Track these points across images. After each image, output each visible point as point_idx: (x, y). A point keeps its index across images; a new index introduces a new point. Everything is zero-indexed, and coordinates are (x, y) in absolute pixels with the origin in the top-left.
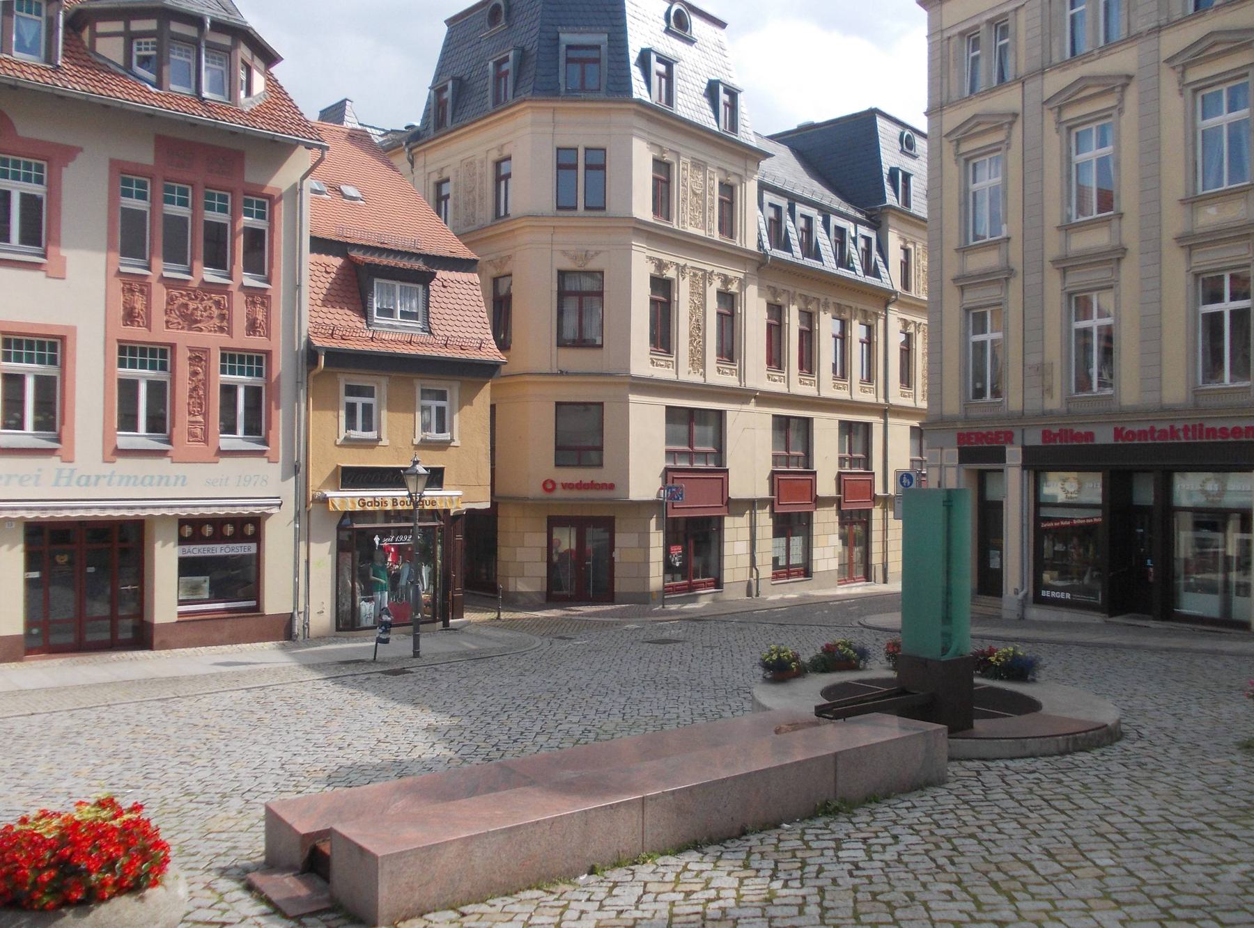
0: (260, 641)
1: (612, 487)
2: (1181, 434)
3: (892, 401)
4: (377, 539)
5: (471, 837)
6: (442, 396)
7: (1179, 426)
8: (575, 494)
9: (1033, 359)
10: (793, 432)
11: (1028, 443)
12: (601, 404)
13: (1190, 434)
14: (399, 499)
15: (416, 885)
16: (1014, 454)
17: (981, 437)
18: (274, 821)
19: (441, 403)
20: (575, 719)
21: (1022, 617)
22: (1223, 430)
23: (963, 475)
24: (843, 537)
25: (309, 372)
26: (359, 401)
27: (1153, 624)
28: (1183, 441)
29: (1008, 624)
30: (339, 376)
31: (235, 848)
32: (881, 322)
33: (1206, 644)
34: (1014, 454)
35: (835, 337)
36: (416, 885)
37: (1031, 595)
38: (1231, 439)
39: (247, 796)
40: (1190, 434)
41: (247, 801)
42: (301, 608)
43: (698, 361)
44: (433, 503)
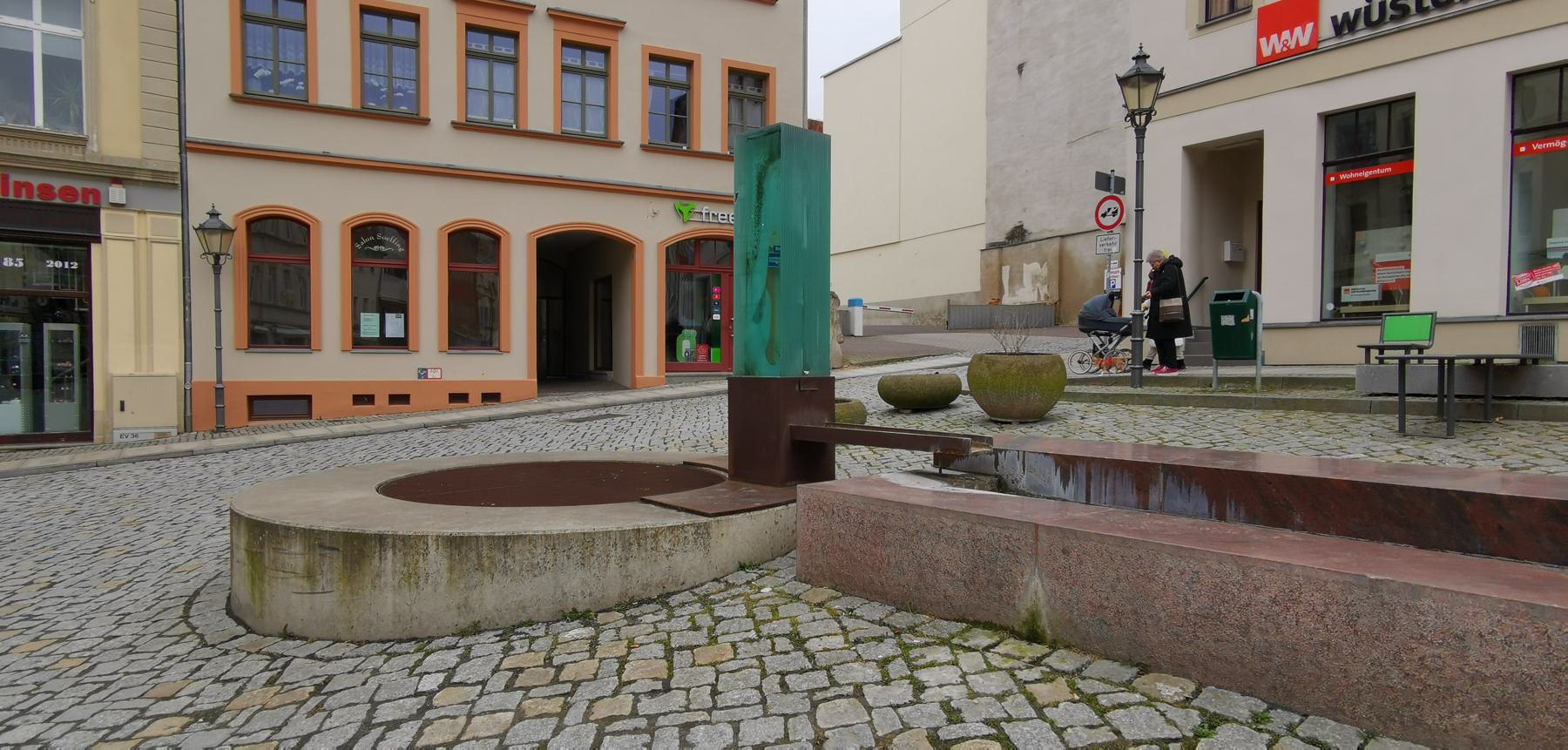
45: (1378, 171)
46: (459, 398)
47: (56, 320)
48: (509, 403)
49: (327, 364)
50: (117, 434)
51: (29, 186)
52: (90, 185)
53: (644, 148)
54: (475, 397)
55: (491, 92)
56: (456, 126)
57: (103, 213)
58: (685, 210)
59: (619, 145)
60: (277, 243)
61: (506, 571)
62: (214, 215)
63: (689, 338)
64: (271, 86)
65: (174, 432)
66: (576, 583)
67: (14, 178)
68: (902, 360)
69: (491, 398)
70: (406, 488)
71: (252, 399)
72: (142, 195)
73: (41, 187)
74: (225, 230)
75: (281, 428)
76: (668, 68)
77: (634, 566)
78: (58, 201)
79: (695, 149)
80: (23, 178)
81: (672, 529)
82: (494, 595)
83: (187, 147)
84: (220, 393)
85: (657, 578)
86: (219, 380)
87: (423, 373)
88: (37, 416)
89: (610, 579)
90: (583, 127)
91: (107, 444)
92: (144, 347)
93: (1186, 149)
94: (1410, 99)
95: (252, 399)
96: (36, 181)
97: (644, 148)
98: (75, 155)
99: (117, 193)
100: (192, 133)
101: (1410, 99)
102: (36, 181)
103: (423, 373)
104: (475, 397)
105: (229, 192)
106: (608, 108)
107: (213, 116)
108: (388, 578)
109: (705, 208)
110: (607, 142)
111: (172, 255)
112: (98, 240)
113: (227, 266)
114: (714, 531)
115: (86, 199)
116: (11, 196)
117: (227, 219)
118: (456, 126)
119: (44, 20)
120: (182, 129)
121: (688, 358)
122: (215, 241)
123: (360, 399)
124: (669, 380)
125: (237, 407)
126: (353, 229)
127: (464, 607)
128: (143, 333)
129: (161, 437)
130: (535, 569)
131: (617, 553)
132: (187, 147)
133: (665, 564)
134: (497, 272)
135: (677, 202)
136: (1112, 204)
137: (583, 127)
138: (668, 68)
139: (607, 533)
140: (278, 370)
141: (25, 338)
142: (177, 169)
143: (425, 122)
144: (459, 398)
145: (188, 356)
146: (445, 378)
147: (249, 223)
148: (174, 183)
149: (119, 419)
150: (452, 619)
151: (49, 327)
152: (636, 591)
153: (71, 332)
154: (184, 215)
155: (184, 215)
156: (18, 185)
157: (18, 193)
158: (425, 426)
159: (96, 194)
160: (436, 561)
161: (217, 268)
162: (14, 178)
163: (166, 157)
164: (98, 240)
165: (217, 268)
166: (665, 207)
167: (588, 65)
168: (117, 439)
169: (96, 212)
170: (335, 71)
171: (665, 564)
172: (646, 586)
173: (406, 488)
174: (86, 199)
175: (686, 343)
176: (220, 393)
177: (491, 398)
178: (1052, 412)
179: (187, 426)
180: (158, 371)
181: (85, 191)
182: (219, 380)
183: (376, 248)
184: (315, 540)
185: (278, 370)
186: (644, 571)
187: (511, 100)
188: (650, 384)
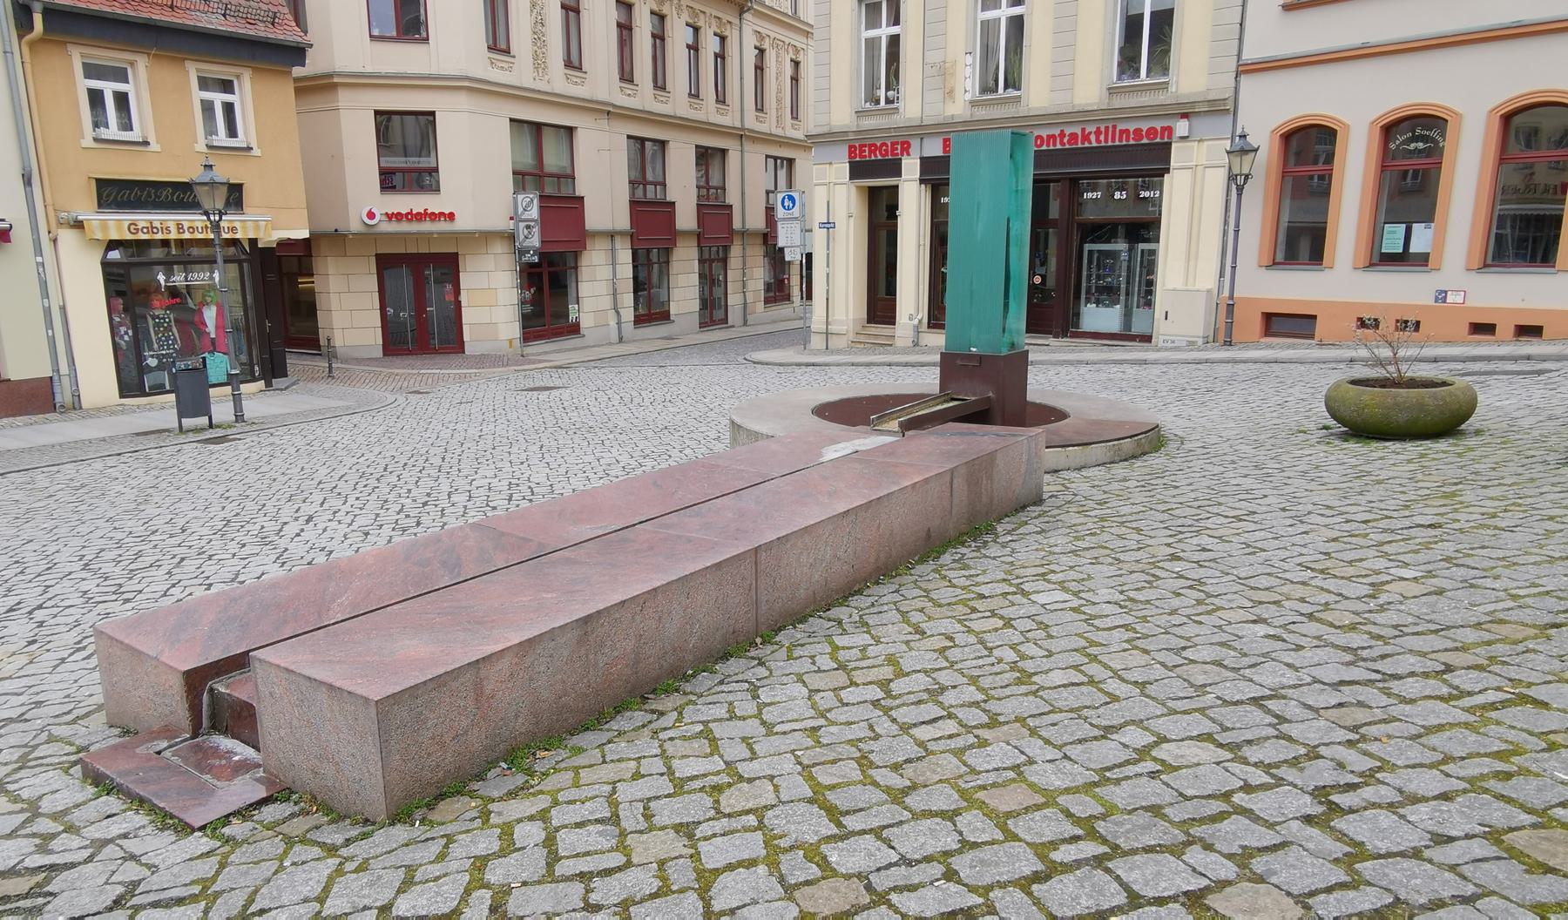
0: (7, 416)
1: (451, 216)
2: (1093, 138)
3: (747, 126)
4: (161, 278)
5: (530, 642)
6: (227, 87)
7: (1091, 128)
8: (405, 227)
9: (933, 57)
10: (646, 155)
11: (925, 155)
12: (433, 114)
13: (1102, 138)
14: (186, 225)
15: (447, 738)
16: (911, 167)
17: (873, 148)
18: (113, 651)
19: (228, 98)
20: (490, 474)
21: (916, 344)
22: (1138, 132)
23: (853, 190)
24: (701, 276)
25: (20, 37)
26: (109, 88)
27: (1051, 341)
28: (1094, 144)
29: (904, 351)
30: (70, 47)
31: (39, 704)
32: (736, 33)
33: (1119, 354)
34: (911, 167)
35: (689, 47)
36: (447, 738)
37: (925, 320)
38: (1145, 141)
39: (39, 615)
40: (1102, 138)
41: (41, 624)
42: (64, 369)
43: (540, 64)
44: (233, 229)
46: (1483, 329)
47: (1093, 242)
48: (1321, 345)
49: (1339, 283)
51: (1127, 131)
52: (1166, 124)
54: (1505, 329)
57: (1174, 146)
65: (1200, 342)
69: (1528, 331)
71: (1269, 318)
72: (1202, 125)
73: (1149, 130)
75: (1293, 347)
80: (1036, 133)
86: (1231, 297)
87: (1441, 296)
99: (1181, 127)
103: (1441, 296)
104: (1505, 329)
105: (1269, 110)
120: (1239, 55)
123: (1362, 323)
128: (1191, 255)
129: (1191, 343)
134: (1330, 158)
140: (1295, 288)
141: (1124, 256)
143: (575, 329)
144: (1483, 329)
146: (1469, 304)
148: (1222, 109)
153: (1091, 252)
158: (890, 365)
159: (1170, 130)
163: (1222, 85)
177: (1528, 331)
182: (1231, 297)
183: (1413, 146)
185: (1295, 288)
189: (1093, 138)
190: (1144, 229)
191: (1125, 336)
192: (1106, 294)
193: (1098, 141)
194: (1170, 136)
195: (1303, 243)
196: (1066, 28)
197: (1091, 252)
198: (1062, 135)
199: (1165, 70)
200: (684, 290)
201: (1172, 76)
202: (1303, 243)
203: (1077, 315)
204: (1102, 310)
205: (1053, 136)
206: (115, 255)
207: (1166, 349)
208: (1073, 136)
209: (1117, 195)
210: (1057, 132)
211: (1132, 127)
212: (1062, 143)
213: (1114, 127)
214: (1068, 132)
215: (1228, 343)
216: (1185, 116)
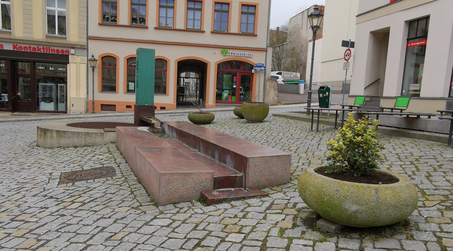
2: (42, 50)
13: (45, 50)
27: (31, 114)
45: (419, 43)
50: (72, 112)
51: (54, 50)
52: (67, 49)
53: (212, 32)
55: (166, 17)
56: (156, 28)
58: (224, 52)
59: (204, 32)
60: (109, 63)
61: (65, 137)
62: (93, 56)
63: (226, 93)
64: (109, 19)
65: (84, 112)
66: (76, 141)
67: (51, 48)
68: (301, 103)
70: (68, 125)
71: (102, 105)
72: (78, 51)
74: (95, 60)
76: (222, 6)
77: (87, 139)
78: (60, 53)
79: (229, 32)
81: (95, 133)
82: (63, 141)
83: (89, 38)
84: (93, 103)
85: (92, 142)
86: (93, 100)
88: (57, 107)
89: (82, 141)
90: (194, 26)
91: (70, 114)
92: (78, 90)
93: (371, 32)
94: (427, 18)
95: (102, 105)
96: (56, 49)
97: (212, 32)
98: (64, 42)
99: (72, 51)
100: (89, 35)
101: (427, 18)
102: (56, 49)
105: (98, 50)
106: (201, 20)
107: (95, 30)
108: (49, 137)
109: (231, 51)
110: (201, 31)
111: (85, 66)
112: (68, 63)
113: (96, 70)
114: (105, 134)
115: (66, 53)
116: (51, 53)
117: (96, 57)
118: (156, 28)
119: (54, 11)
121: (226, 99)
122: (92, 64)
124: (216, 106)
125: (98, 107)
126: (128, 59)
127: (59, 143)
128: (78, 88)
130: (69, 138)
131: (84, 136)
132: (89, 38)
133: (93, 140)
135: (222, 50)
136: (348, 52)
137: (194, 26)
138: (222, 6)
139: (82, 132)
140: (108, 97)
142: (86, 44)
143: (147, 28)
145: (87, 94)
147: (102, 58)
148: (85, 48)
149: (72, 109)
150: (57, 145)
151: (59, 85)
152: (88, 144)
154: (87, 56)
155: (87, 56)
156: (52, 50)
157: (52, 52)
159: (68, 51)
160: (55, 134)
161: (93, 70)
162: (51, 48)
163: (83, 41)
164: (68, 63)
165: (93, 70)
166: (218, 51)
167: (196, 7)
168: (71, 113)
169: (68, 56)
170: (124, 16)
171: (93, 140)
172: (89, 143)
173: (68, 125)
174: (66, 53)
175: (225, 94)
176: (93, 103)
178: (265, 119)
179: (87, 111)
180: (81, 97)
181: (66, 51)
182: (93, 100)
184: (58, 131)
185: (108, 97)
186: (89, 140)
187: (172, 19)
188: (211, 107)
189: (42, 50)
190: (64, 80)
191: (56, 112)
192: (48, 100)
193: (44, 51)
194: (68, 53)
195: (109, 86)
196: (28, 13)
197: (61, 87)
198: (30, 47)
199: (65, 33)
200: (245, 10)
201: (67, 35)
202: (109, 86)
203: (38, 105)
204: (46, 104)
205: (26, 47)
206: (367, 99)
207: (74, 115)
208: (34, 49)
209: (50, 69)
210: (28, 46)
211: (56, 49)
212: (30, 50)
213: (49, 48)
214: (32, 46)
215: (93, 113)
216: (73, 48)
